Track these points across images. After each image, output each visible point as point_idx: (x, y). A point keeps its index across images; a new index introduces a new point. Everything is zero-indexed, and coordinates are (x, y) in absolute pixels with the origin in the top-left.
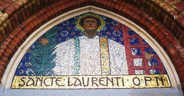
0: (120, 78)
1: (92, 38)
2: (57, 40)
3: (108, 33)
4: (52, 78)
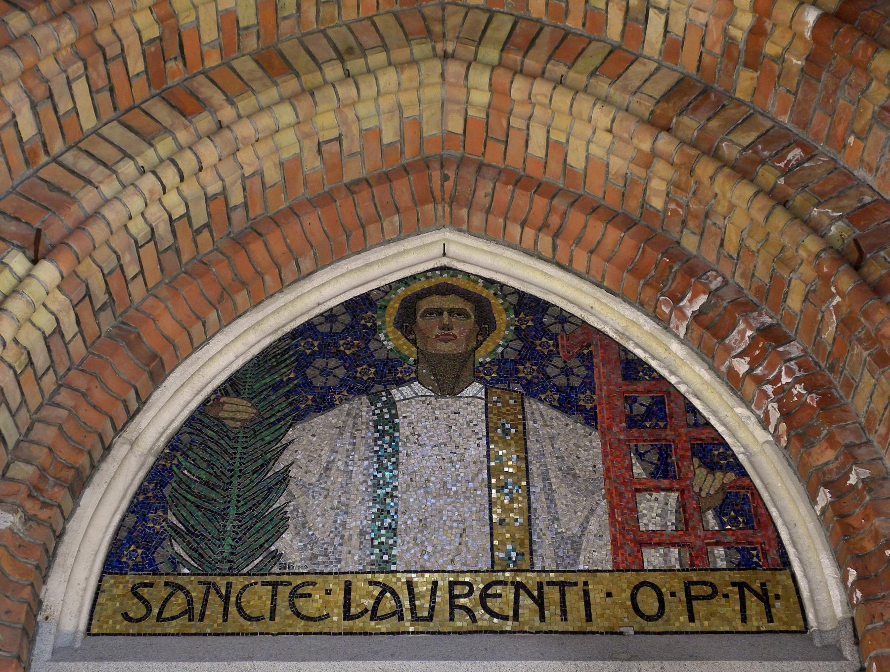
0: (576, 584)
1: (453, 393)
2: (291, 404)
3: (526, 371)
4: (275, 585)
